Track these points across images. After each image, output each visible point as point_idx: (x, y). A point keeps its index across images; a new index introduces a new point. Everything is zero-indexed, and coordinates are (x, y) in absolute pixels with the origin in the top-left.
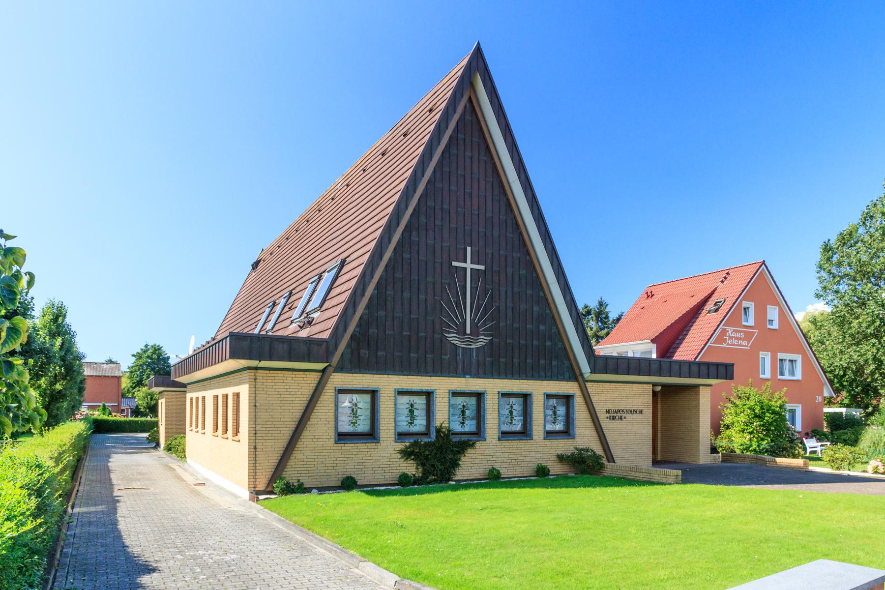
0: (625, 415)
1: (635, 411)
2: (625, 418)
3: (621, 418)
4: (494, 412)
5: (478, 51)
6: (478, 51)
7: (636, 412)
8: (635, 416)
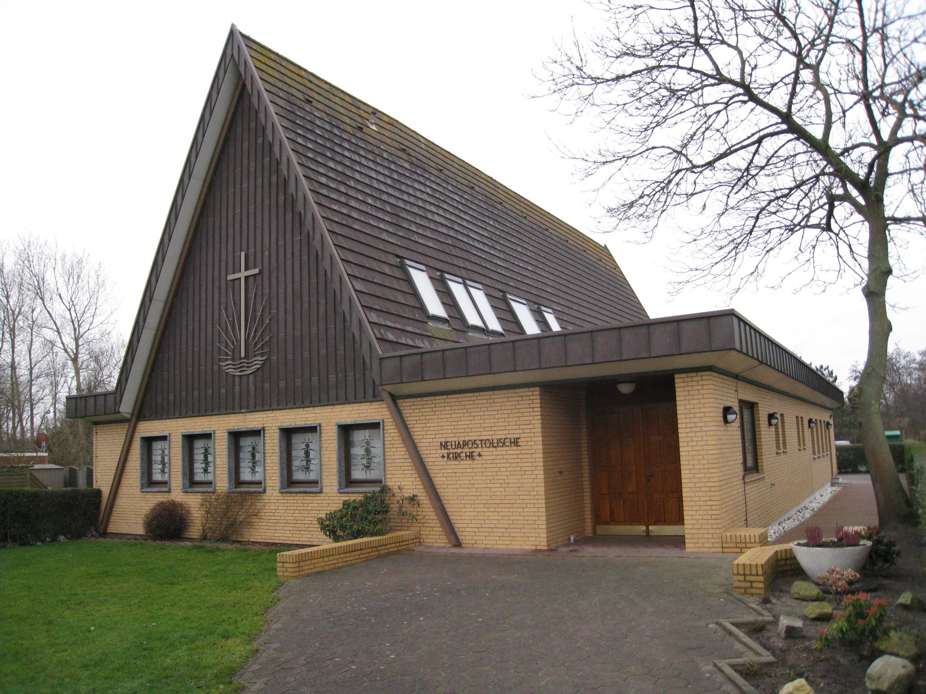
0: (480, 450)
1: (502, 443)
2: (480, 455)
3: (471, 456)
4: (274, 455)
5: (233, 26)
6: (233, 26)
7: (504, 443)
8: (501, 451)
